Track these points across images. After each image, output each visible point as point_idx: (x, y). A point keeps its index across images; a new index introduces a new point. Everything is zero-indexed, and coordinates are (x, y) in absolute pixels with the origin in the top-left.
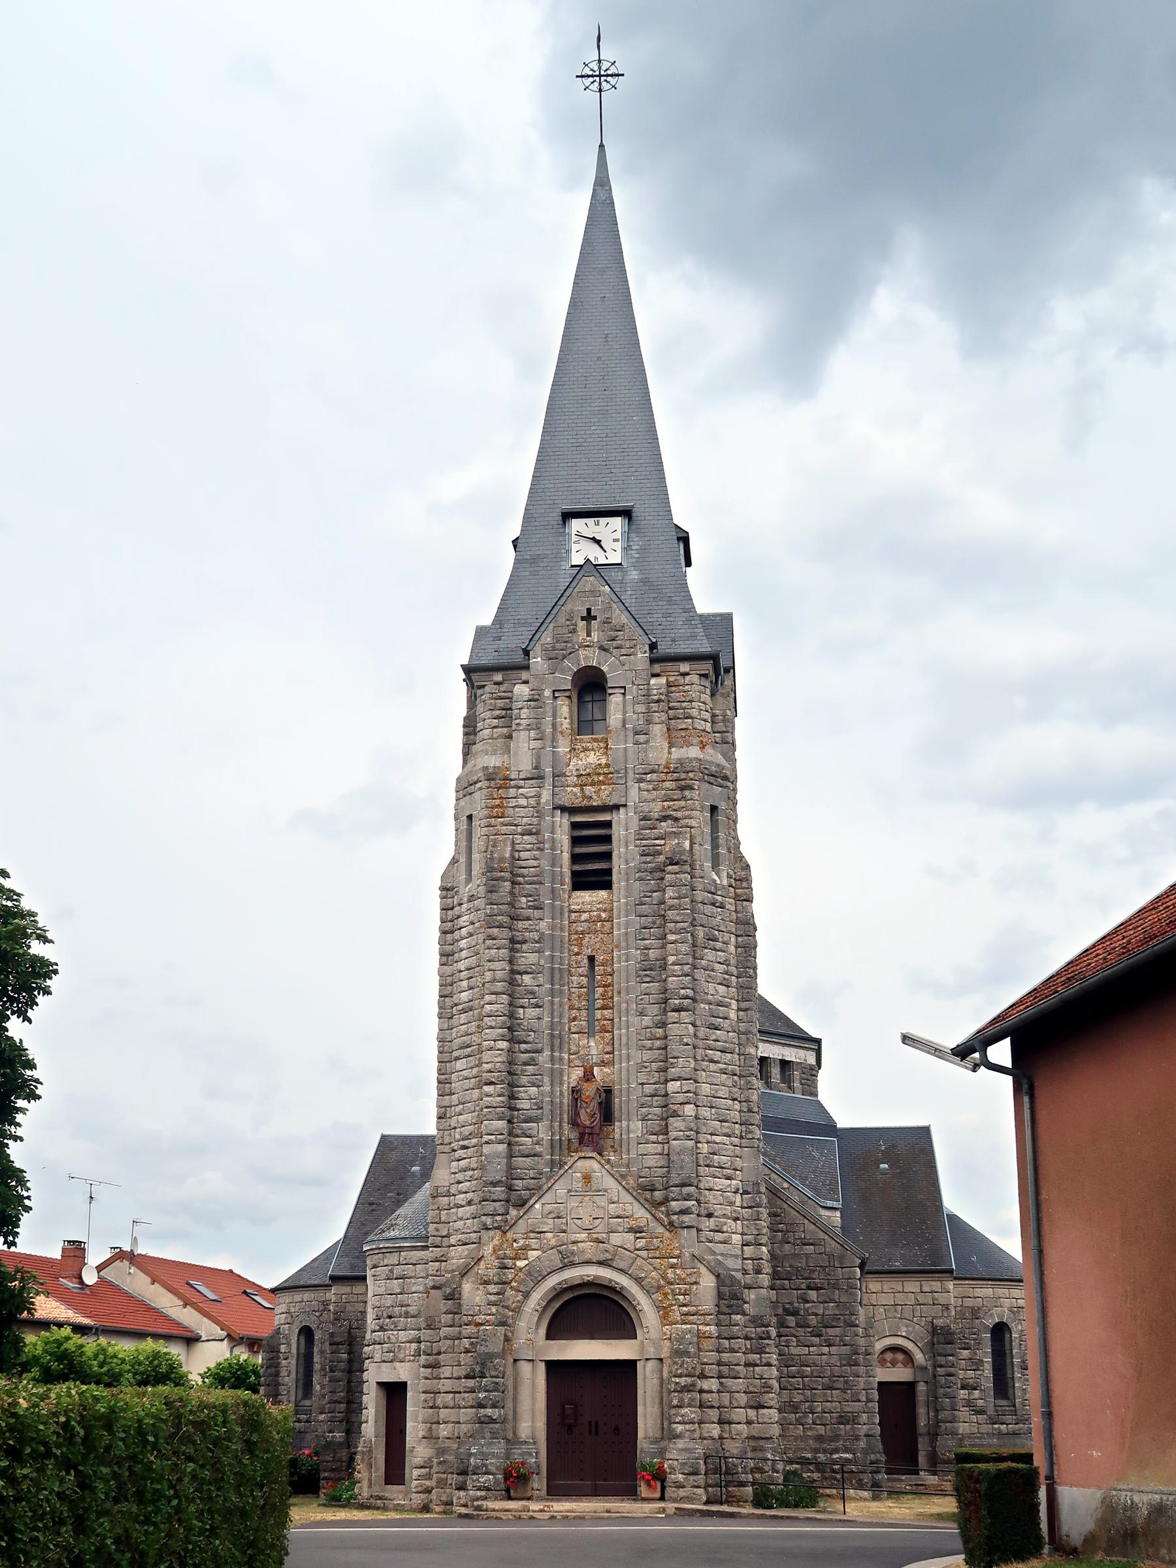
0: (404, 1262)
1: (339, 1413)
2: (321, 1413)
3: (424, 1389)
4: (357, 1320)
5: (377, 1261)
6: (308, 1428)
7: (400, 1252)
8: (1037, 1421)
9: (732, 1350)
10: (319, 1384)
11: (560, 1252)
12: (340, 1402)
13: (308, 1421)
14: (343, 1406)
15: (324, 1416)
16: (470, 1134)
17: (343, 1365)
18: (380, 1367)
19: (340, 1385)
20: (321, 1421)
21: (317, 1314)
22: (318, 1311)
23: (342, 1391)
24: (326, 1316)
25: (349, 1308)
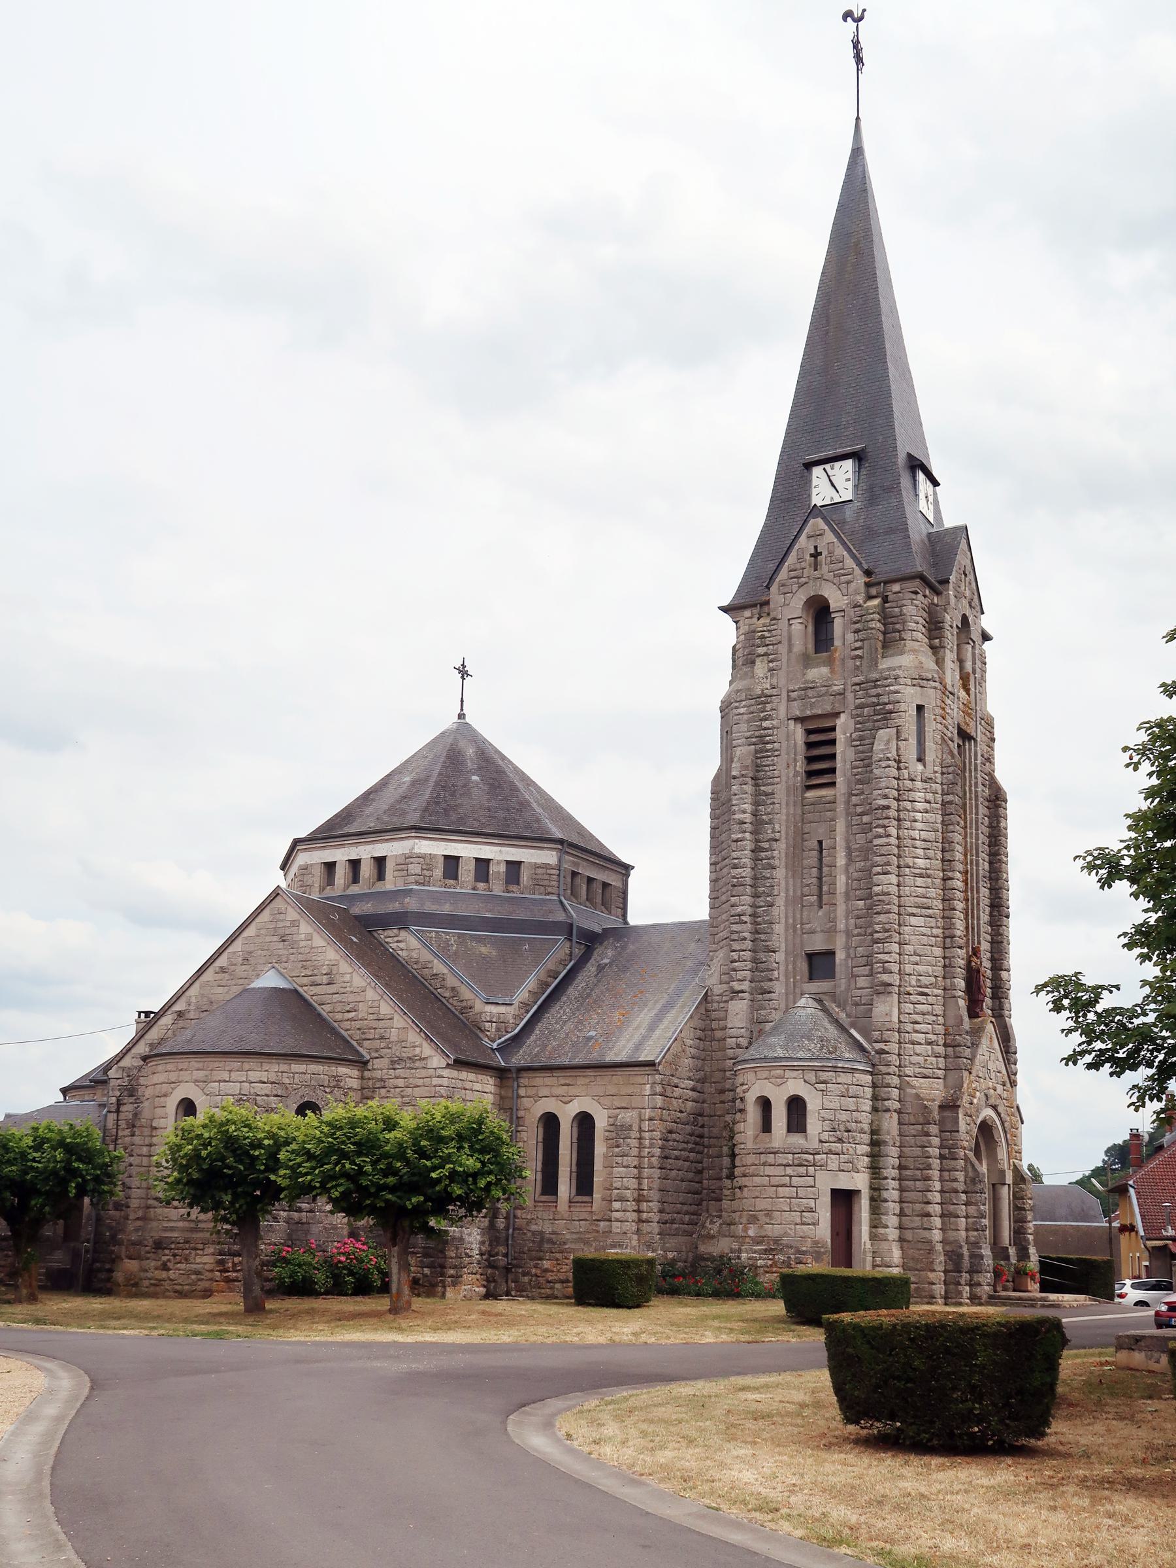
13: (311, 1211)
18: (837, 1176)
22: (328, 1086)
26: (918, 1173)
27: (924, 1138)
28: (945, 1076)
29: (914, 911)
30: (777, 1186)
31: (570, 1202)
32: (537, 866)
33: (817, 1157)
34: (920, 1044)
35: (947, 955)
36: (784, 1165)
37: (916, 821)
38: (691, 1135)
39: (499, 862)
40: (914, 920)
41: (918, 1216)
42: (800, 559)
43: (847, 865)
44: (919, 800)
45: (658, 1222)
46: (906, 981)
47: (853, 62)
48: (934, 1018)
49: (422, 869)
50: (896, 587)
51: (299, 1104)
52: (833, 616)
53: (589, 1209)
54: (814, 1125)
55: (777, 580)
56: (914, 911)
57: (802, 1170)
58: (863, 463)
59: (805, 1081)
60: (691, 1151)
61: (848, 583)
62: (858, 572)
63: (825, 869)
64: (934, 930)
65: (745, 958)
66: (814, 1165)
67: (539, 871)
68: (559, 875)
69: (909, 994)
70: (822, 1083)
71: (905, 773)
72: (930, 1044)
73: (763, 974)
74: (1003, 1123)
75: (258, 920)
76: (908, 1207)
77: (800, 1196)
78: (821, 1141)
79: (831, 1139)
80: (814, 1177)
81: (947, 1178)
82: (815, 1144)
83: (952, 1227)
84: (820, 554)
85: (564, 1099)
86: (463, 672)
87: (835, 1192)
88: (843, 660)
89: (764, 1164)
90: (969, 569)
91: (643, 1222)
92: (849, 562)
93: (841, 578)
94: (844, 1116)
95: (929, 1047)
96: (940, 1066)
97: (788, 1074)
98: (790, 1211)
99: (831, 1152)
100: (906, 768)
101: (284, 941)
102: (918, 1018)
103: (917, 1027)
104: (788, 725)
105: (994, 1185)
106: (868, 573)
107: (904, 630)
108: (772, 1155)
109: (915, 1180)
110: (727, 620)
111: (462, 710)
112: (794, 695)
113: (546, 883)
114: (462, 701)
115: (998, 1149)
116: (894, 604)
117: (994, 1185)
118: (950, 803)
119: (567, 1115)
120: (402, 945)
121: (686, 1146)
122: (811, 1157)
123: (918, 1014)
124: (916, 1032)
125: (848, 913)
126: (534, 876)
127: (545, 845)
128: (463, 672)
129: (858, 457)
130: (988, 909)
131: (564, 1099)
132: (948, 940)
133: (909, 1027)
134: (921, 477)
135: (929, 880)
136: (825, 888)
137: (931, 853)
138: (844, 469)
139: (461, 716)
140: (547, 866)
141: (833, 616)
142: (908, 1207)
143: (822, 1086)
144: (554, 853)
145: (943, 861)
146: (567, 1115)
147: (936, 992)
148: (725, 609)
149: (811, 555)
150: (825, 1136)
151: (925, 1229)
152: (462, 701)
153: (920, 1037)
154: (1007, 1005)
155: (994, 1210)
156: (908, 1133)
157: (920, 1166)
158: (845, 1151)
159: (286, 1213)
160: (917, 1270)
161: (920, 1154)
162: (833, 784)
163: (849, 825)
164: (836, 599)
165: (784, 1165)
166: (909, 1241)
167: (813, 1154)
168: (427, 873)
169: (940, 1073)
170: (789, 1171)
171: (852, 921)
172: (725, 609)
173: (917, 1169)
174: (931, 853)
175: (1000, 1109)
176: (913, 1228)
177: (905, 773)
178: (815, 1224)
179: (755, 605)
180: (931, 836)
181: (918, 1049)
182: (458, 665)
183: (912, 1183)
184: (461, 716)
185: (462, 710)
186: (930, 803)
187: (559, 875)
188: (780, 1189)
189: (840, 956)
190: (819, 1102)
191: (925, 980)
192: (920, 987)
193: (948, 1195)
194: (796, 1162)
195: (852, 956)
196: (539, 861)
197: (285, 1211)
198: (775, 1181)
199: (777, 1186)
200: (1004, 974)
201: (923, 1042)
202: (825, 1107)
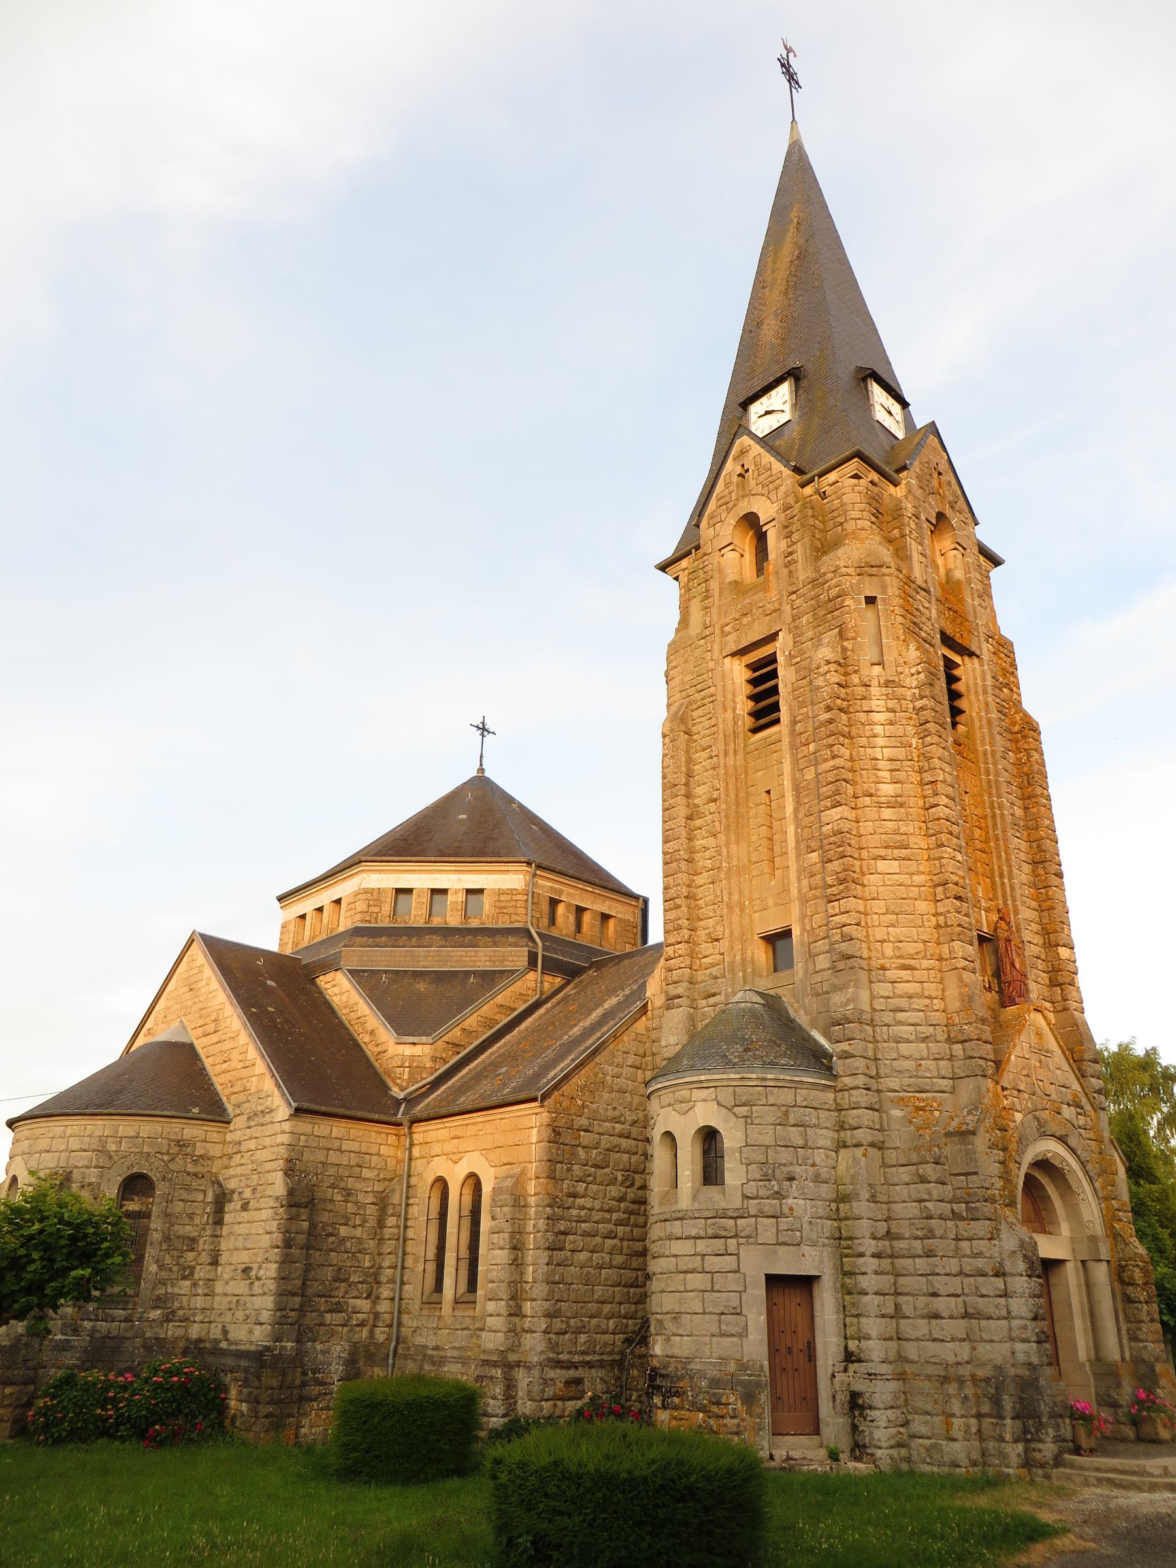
0: (805, 1104)
1: (292, 1310)
2: (155, 1308)
3: (876, 1289)
4: (316, 1174)
5: (756, 1096)
6: (126, 1330)
7: (674, 1092)
8: (1124, 1333)
9: (976, 1255)
10: (157, 1262)
11: (1038, 1119)
12: (294, 1295)
13: (127, 1320)
14: (297, 1299)
15: (159, 1312)
16: (917, 953)
17: (302, 1238)
18: (775, 1252)
19: (296, 1268)
20: (154, 1320)
21: (166, 1158)
22: (168, 1153)
23: (297, 1278)
24: (180, 1162)
25: (307, 1156)
26: (917, 1244)
27: (921, 1187)
28: (953, 1088)
29: (882, 852)
30: (686, 1272)
31: (456, 1302)
32: (500, 892)
33: (741, 1222)
34: (909, 1041)
35: (939, 911)
36: (695, 1238)
37: (875, 736)
38: (620, 1200)
39: (457, 891)
40: (882, 865)
41: (923, 1317)
42: (727, 485)
43: (796, 810)
44: (878, 709)
45: (545, 1332)
46: (877, 951)
47: (783, 80)
48: (927, 1001)
49: (369, 906)
50: (832, 476)
51: (124, 1176)
52: (764, 529)
53: (471, 1313)
54: (734, 1173)
55: (706, 514)
56: (882, 852)
57: (718, 1244)
58: (801, 382)
59: (719, 1104)
60: (619, 1223)
61: (777, 488)
62: (787, 472)
63: (776, 825)
64: (915, 877)
65: (680, 952)
66: (736, 1236)
67: (503, 898)
68: (526, 901)
69: (883, 968)
70: (744, 1105)
71: (855, 679)
72: (924, 1040)
73: (707, 972)
74: (1083, 1164)
75: (178, 971)
76: (907, 1303)
77: (717, 1287)
78: (746, 1197)
79: (761, 1193)
80: (737, 1255)
81: (968, 1252)
82: (737, 1202)
83: (985, 1336)
84: (747, 471)
85: (454, 1157)
86: (483, 729)
87: (774, 1282)
88: (777, 573)
89: (670, 1238)
90: (943, 467)
91: (527, 1332)
92: (778, 466)
93: (770, 486)
94: (785, 1156)
95: (923, 1045)
96: (943, 1073)
97: (698, 1094)
98: (704, 1313)
99: (760, 1214)
100: (856, 672)
101: (191, 990)
102: (903, 1003)
103: (901, 1016)
104: (723, 664)
105: (1083, 1262)
106: (798, 470)
107: (846, 521)
108: (678, 1223)
109: (914, 1257)
110: (666, 579)
111: (481, 765)
112: (727, 629)
113: (511, 910)
114: (481, 757)
115: (1082, 1206)
116: (834, 497)
117: (1083, 1262)
118: (922, 708)
119: (456, 1178)
120: (336, 990)
121: (607, 1216)
122: (732, 1222)
123: (900, 996)
124: (901, 1023)
125: (801, 871)
126: (498, 904)
127: (510, 868)
128: (483, 729)
129: (795, 375)
130: (1027, 868)
131: (454, 1157)
132: (940, 889)
133: (888, 1017)
134: (876, 390)
135: (903, 810)
136: (777, 849)
137: (901, 775)
138: (780, 394)
139: (481, 770)
140: (511, 892)
141: (764, 529)
142: (907, 1303)
143: (743, 1110)
144: (521, 877)
145: (922, 783)
146: (456, 1178)
147: (926, 963)
148: (663, 567)
149: (740, 475)
150: (751, 1189)
151: (934, 1340)
152: (481, 757)
153: (905, 1031)
154: (1075, 994)
155: (1090, 1302)
156: (896, 1180)
157: (920, 1233)
158: (786, 1211)
159: (91, 1324)
160: (928, 1413)
161: (917, 1212)
162: (777, 721)
163: (795, 761)
164: (765, 510)
165: (695, 1238)
166: (913, 1362)
167: (735, 1218)
168: (376, 909)
169: (945, 1084)
170: (701, 1246)
171: (805, 882)
172: (663, 567)
173: (916, 1238)
174: (901, 775)
175: (1072, 1142)
176: (917, 1339)
177: (855, 679)
178: (743, 1334)
179: (690, 553)
180: (900, 753)
181: (905, 1048)
182: (478, 722)
183: (910, 1261)
184: (481, 770)
185: (481, 765)
186: (895, 712)
187: (526, 901)
188: (689, 1276)
189: (796, 932)
190: (740, 1134)
191: (911, 948)
192: (898, 957)
193: (972, 1279)
194: (710, 1232)
195: (808, 928)
196: (504, 887)
197: (90, 1320)
198: (684, 1264)
199: (686, 1272)
200: (1063, 952)
201: (913, 1037)
202: (750, 1142)
